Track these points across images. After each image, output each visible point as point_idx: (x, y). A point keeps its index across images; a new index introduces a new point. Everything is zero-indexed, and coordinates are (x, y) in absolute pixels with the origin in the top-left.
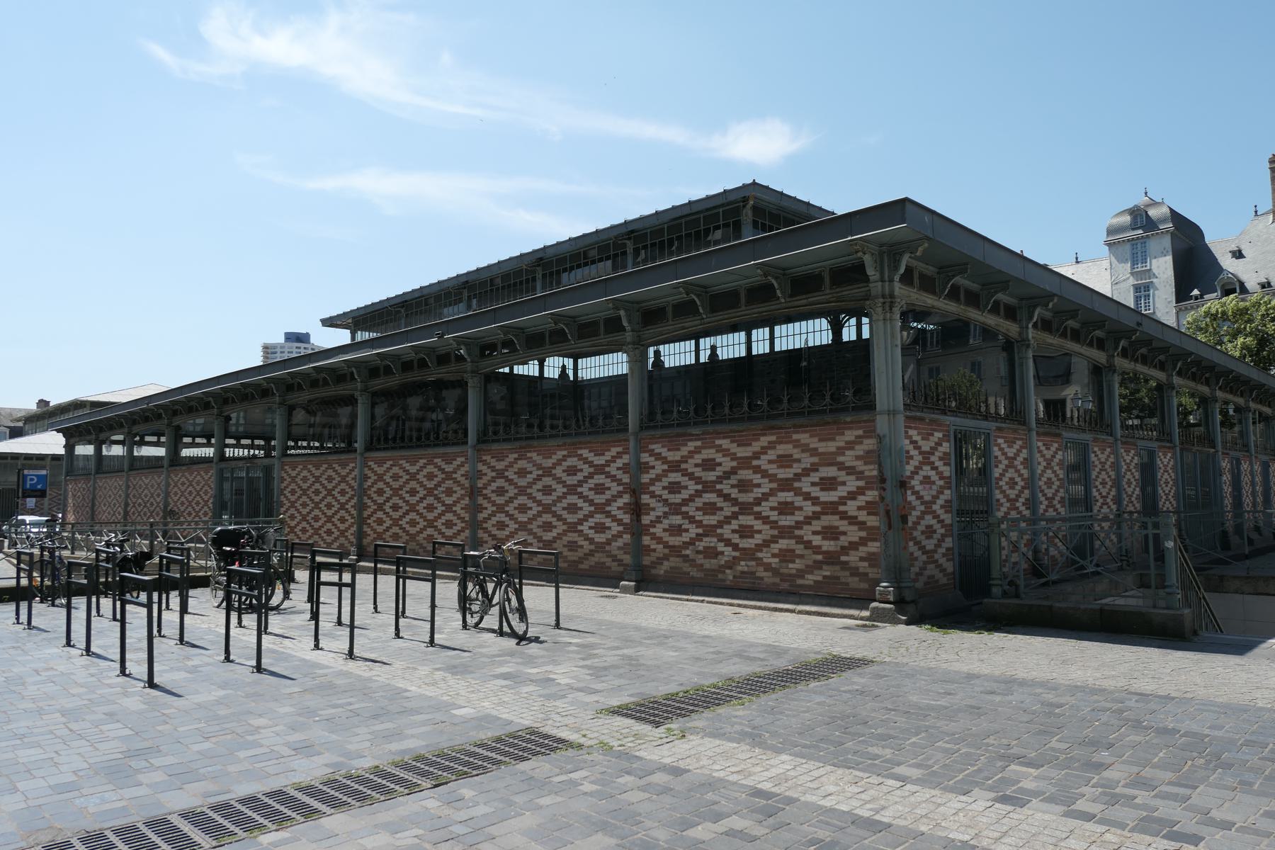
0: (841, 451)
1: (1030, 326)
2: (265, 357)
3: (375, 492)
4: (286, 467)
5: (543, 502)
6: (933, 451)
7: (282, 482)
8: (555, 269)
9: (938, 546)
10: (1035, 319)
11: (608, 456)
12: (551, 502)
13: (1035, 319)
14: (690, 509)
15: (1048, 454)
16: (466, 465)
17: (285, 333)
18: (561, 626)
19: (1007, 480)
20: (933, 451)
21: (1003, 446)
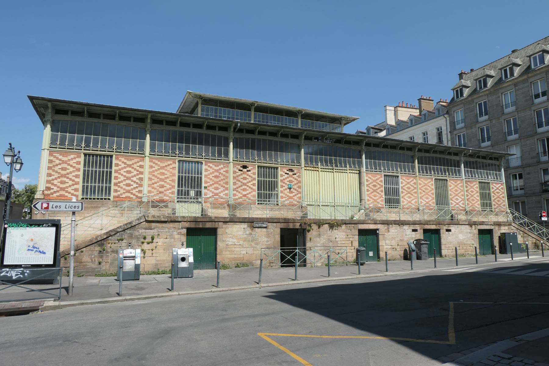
0: (69, 160)
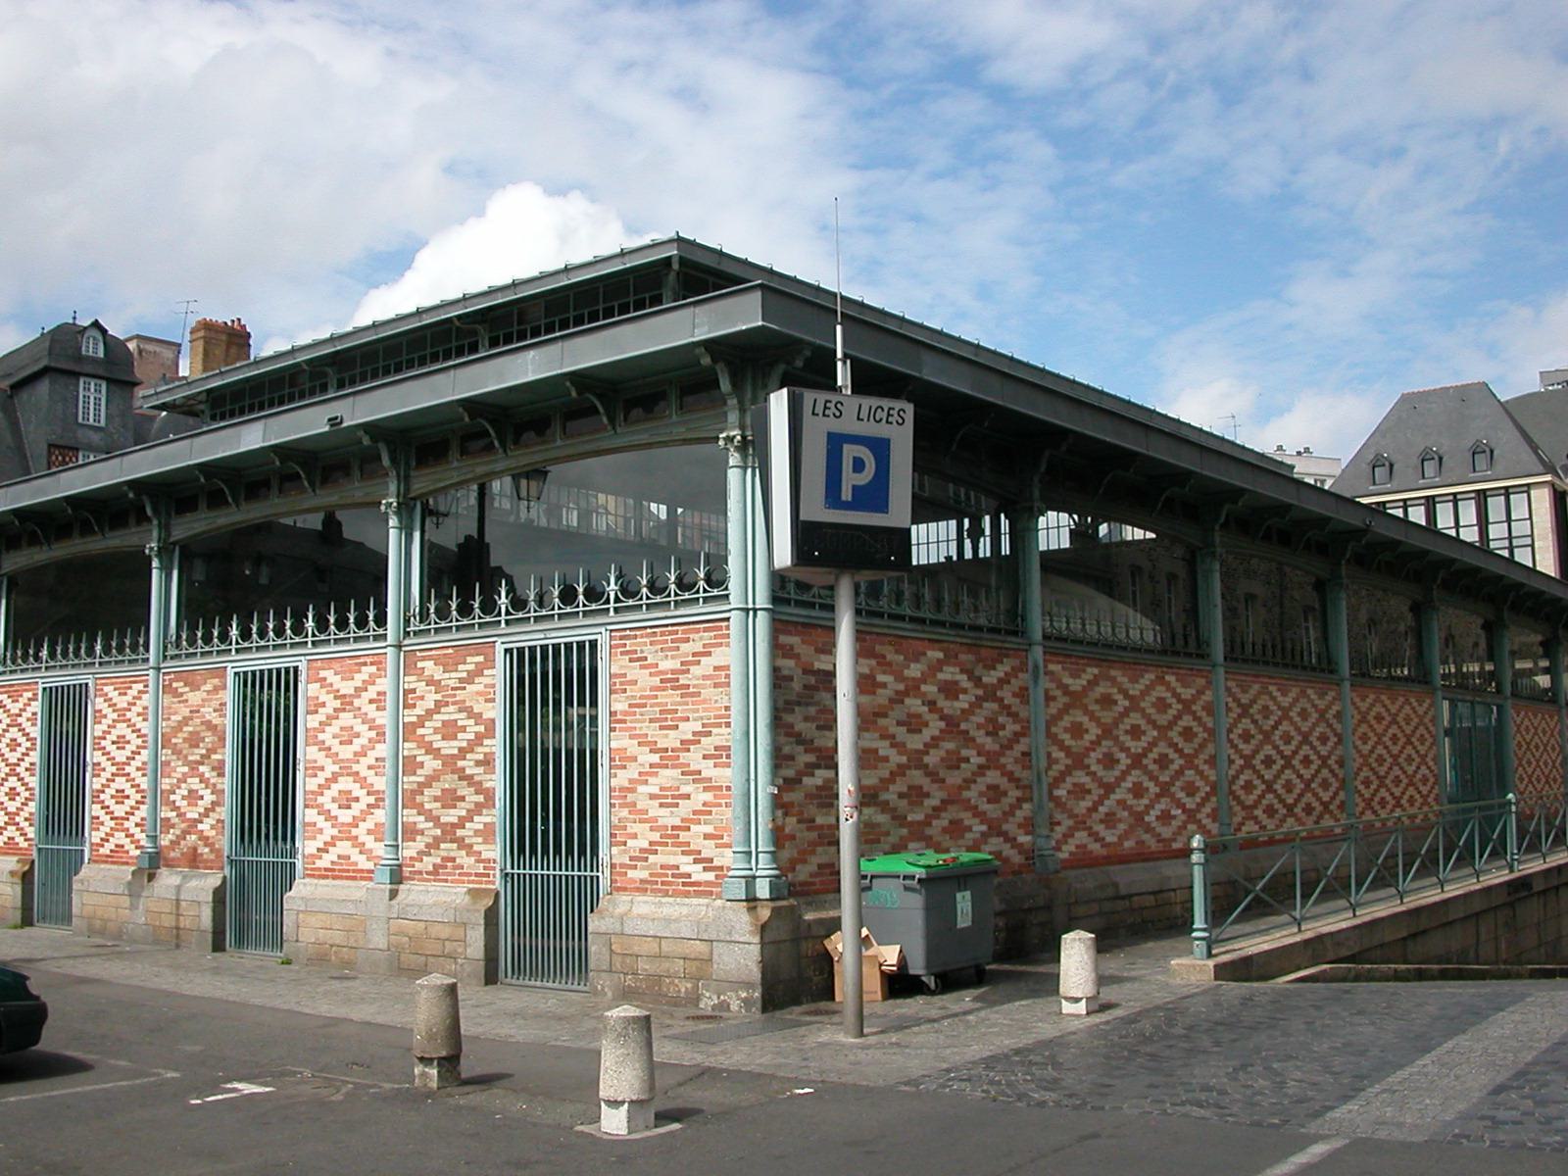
1: (1343, 562)
2: (1377, 462)
3: (1066, 730)
4: (106, 689)
5: (443, 752)
6: (1194, 700)
7: (1338, 712)
8: (228, 407)
9: (1333, 798)
10: (1348, 556)
11: (359, 679)
12: (456, 751)
13: (1348, 556)
14: (694, 758)
15: (1364, 706)
16: (1207, 692)
17: (829, 434)
18: (864, 894)
19: (1240, 731)
20: (1194, 700)
21: (1275, 694)
